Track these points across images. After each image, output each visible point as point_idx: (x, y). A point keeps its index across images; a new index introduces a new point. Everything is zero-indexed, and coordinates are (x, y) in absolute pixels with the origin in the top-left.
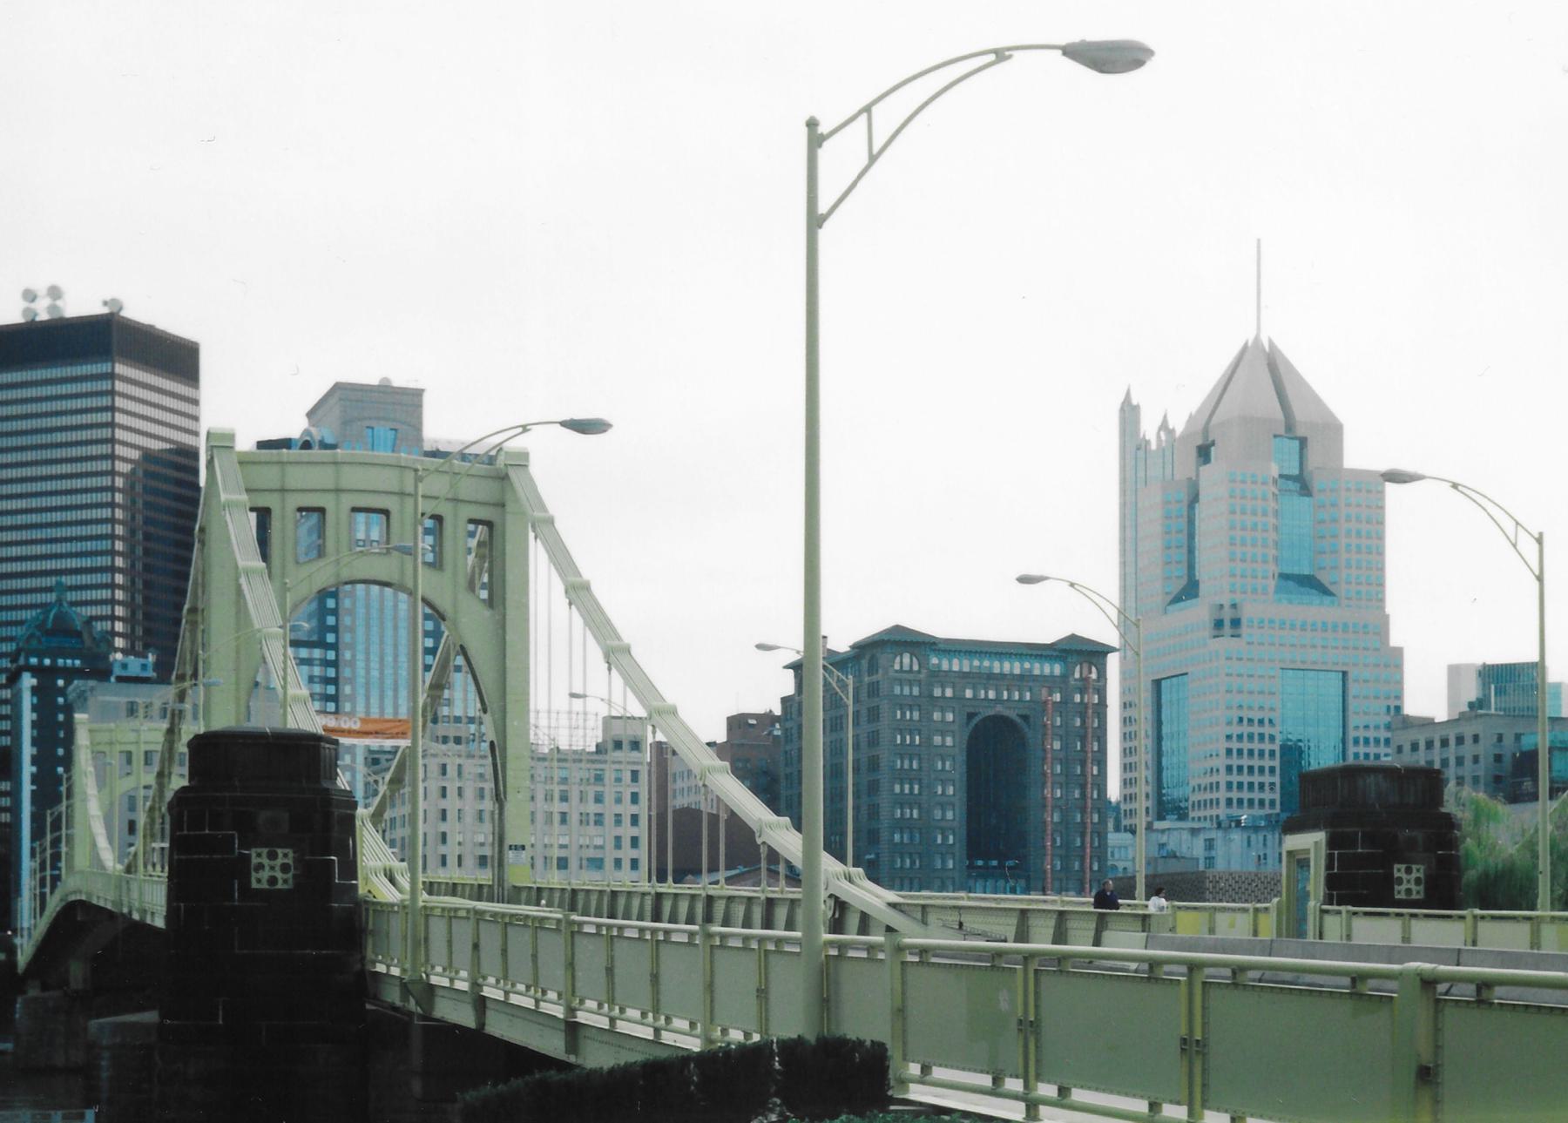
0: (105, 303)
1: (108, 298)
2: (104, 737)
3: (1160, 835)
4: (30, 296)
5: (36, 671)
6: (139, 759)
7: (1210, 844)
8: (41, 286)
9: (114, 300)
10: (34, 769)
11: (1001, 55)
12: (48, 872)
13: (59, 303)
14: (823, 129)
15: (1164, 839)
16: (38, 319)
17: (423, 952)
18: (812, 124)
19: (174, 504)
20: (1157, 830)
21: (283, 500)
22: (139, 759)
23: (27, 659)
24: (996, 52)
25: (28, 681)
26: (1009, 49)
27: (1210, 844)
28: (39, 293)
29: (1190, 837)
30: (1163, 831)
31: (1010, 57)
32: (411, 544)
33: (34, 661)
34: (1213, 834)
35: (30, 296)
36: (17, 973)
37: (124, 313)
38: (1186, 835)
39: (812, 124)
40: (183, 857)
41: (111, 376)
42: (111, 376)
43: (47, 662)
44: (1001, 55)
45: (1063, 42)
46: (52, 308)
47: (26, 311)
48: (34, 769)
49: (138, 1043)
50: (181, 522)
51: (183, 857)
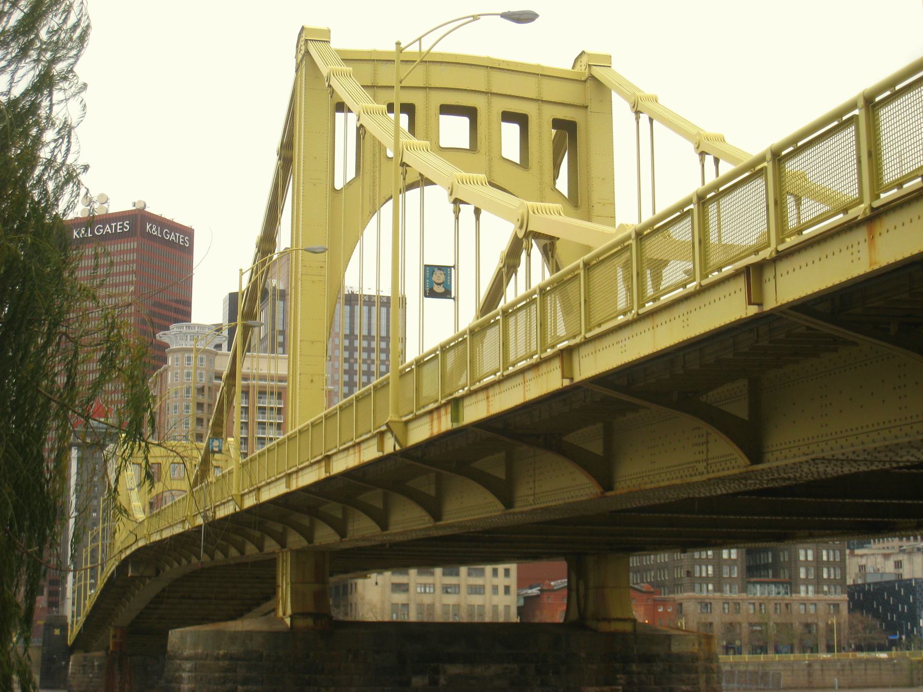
3: (859, 559)
5: (79, 446)
6: (584, 357)
7: (898, 565)
9: (139, 202)
11: (475, 18)
12: (83, 583)
14: (243, 271)
15: (863, 561)
18: (241, 270)
20: (857, 555)
21: (489, 103)
22: (584, 357)
24: (473, 16)
26: (479, 15)
27: (898, 565)
29: (883, 560)
30: (862, 556)
31: (479, 19)
32: (287, 373)
34: (900, 557)
37: (147, 210)
38: (880, 559)
39: (241, 270)
44: (475, 18)
45: (501, 12)
49: (221, 652)
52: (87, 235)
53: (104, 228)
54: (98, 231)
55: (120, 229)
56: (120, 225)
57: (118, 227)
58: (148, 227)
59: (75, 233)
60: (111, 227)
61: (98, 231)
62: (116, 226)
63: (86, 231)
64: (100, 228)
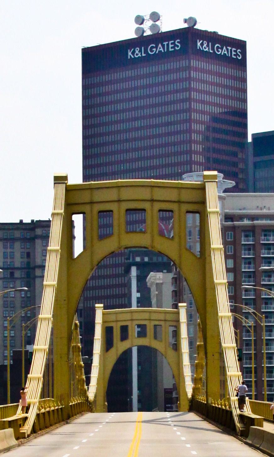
0: (186, 21)
1: (187, 17)
2: (113, 318)
4: (140, 20)
5: (138, 265)
8: (146, 14)
9: (191, 18)
10: (139, 295)
13: (158, 23)
16: (145, 34)
17: (216, 443)
19: (230, 128)
23: (134, 259)
25: (134, 271)
28: (145, 18)
33: (138, 259)
35: (140, 20)
36: (162, 52)
37: (197, 27)
40: (245, 359)
41: (189, 68)
42: (189, 68)
43: (146, 259)
46: (153, 27)
47: (137, 30)
48: (139, 295)
50: (237, 139)
51: (245, 359)
52: (141, 54)
53: (156, 47)
54: (152, 51)
55: (172, 48)
56: (172, 44)
57: (170, 46)
58: (199, 44)
59: (130, 54)
60: (163, 46)
61: (152, 51)
62: (168, 45)
63: (140, 51)
64: (152, 47)
